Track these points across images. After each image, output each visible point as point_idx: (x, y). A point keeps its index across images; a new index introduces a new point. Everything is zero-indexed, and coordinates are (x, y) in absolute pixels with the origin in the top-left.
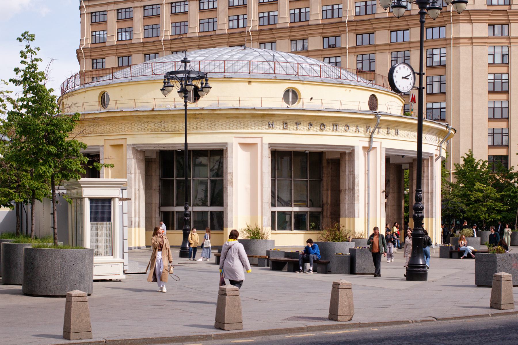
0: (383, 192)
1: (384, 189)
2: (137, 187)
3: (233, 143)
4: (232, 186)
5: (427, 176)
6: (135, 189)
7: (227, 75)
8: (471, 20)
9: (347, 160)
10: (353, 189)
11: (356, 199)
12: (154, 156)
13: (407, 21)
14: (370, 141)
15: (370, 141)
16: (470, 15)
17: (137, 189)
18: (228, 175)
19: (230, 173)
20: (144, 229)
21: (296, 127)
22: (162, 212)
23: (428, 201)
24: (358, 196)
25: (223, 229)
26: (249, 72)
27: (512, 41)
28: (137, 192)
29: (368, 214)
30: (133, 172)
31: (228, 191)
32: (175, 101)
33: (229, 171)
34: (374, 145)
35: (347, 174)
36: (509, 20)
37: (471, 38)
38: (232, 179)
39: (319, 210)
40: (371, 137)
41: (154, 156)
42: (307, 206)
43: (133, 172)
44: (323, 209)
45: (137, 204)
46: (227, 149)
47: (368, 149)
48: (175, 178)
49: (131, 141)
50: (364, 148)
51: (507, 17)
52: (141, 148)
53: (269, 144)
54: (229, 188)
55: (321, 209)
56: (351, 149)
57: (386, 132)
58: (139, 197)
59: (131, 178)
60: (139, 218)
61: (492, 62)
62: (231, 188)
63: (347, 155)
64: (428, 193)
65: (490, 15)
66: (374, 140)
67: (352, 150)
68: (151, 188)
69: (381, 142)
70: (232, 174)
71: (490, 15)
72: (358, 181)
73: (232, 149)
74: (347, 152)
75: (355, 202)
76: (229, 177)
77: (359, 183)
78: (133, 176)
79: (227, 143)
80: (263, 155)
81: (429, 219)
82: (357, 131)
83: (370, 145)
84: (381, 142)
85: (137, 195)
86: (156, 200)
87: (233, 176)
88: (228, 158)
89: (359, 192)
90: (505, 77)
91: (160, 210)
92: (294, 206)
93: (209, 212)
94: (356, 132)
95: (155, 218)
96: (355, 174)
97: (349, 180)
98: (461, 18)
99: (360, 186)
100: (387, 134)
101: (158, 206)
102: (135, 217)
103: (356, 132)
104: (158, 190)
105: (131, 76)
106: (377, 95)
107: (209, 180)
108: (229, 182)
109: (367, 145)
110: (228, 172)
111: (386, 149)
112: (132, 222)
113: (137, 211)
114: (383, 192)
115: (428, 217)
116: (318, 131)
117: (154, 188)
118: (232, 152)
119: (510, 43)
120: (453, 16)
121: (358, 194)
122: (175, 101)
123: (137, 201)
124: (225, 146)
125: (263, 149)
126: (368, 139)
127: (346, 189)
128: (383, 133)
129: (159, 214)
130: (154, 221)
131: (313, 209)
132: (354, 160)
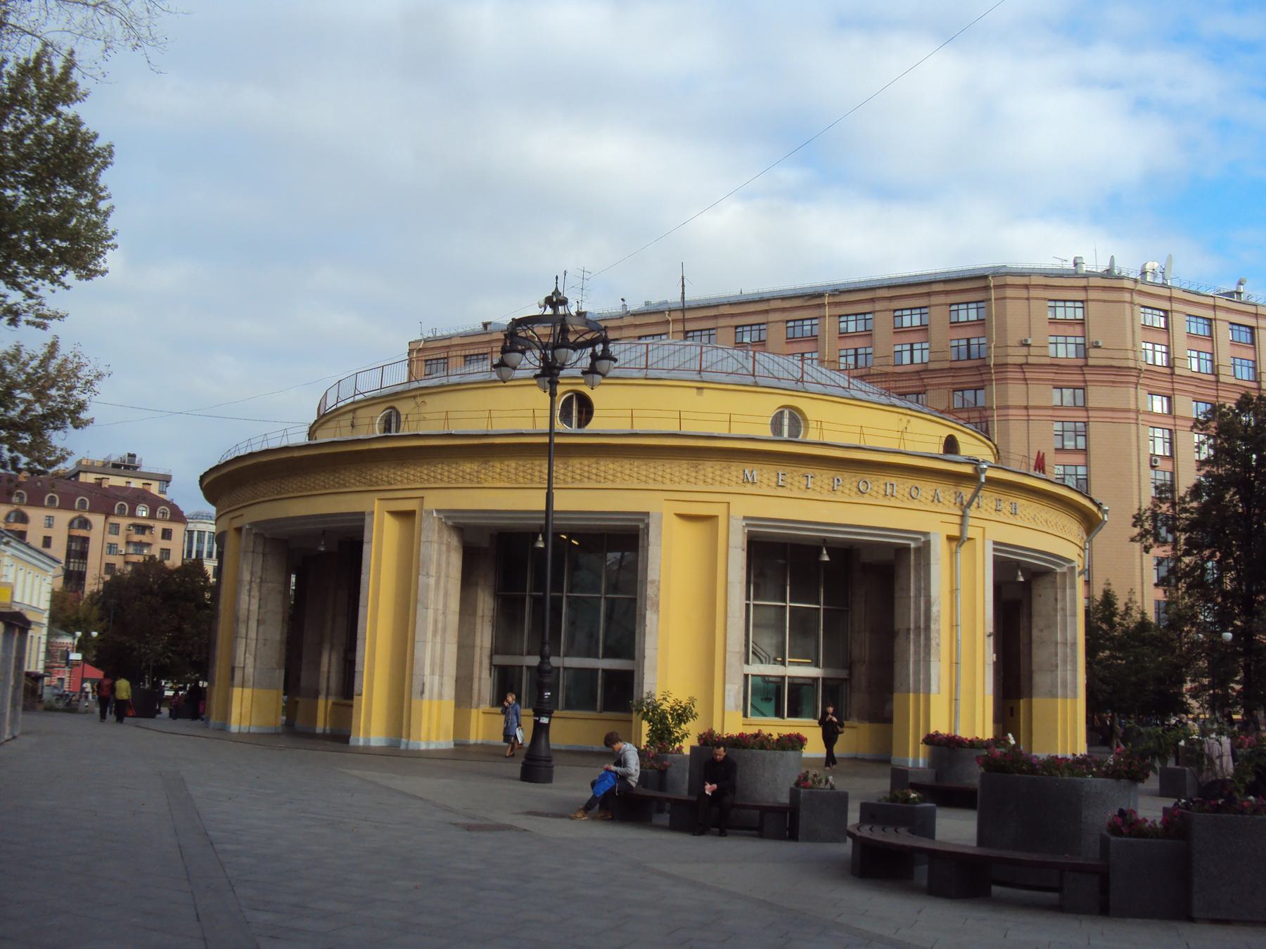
0: (989, 636)
1: (991, 630)
2: (441, 607)
3: (661, 515)
4: (657, 611)
5: (1064, 609)
6: (436, 610)
7: (651, 373)
8: (1025, 379)
9: (912, 563)
10: (928, 628)
11: (933, 651)
12: (485, 543)
13: (922, 379)
14: (962, 525)
15: (962, 525)
16: (1024, 372)
17: (440, 612)
18: (649, 586)
19: (653, 582)
20: (453, 703)
21: (805, 482)
22: (495, 666)
23: (1065, 662)
24: (938, 645)
25: (352, 698)
26: (698, 368)
27: (1091, 413)
28: (440, 618)
29: (957, 685)
30: (433, 571)
31: (648, 622)
32: (534, 417)
33: (652, 575)
34: (970, 532)
35: (912, 594)
36: (1085, 381)
37: (1026, 408)
38: (657, 596)
39: (843, 674)
40: (963, 517)
41: (485, 543)
42: (817, 665)
43: (433, 571)
44: (851, 674)
45: (438, 647)
46: (647, 526)
47: (956, 540)
48: (527, 593)
49: (436, 501)
50: (950, 538)
51: (1082, 376)
52: (456, 521)
53: (745, 518)
54: (650, 616)
55: (847, 672)
56: (923, 539)
57: (994, 507)
58: (444, 629)
59: (428, 585)
60: (441, 676)
61: (1059, 446)
62: (654, 617)
63: (912, 552)
64: (1066, 644)
65: (1056, 373)
66: (971, 521)
67: (924, 542)
68: (474, 613)
69: (984, 528)
70: (657, 584)
71: (1056, 373)
72: (938, 611)
73: (660, 527)
74: (913, 545)
75: (932, 659)
76: (650, 591)
77: (939, 616)
78: (432, 581)
79: (647, 514)
80: (730, 544)
81: (1059, 700)
82: (936, 500)
83: (962, 531)
84: (984, 528)
85: (440, 625)
86: (484, 638)
87: (659, 590)
88: (650, 548)
89: (939, 634)
90: (1081, 470)
91: (491, 664)
92: (789, 665)
93: (600, 672)
94: (933, 501)
95: (480, 679)
96: (932, 594)
97: (918, 608)
98: (1010, 375)
99: (941, 623)
100: (996, 510)
101: (487, 652)
102: (433, 673)
103: (933, 501)
104: (490, 618)
105: (447, 375)
106: (960, 437)
107: (603, 601)
108: (649, 603)
109: (955, 532)
110: (649, 579)
111: (995, 543)
112: (424, 684)
113: (438, 661)
114: (989, 636)
115: (1065, 697)
116: (853, 494)
117: (479, 613)
118: (660, 534)
119: (1088, 417)
120: (995, 373)
121: (937, 641)
122: (534, 417)
123: (439, 639)
124: (643, 520)
125: (731, 529)
126: (957, 520)
127: (909, 630)
128: (988, 509)
129: (488, 672)
130: (476, 687)
131: (832, 673)
132: (928, 564)
